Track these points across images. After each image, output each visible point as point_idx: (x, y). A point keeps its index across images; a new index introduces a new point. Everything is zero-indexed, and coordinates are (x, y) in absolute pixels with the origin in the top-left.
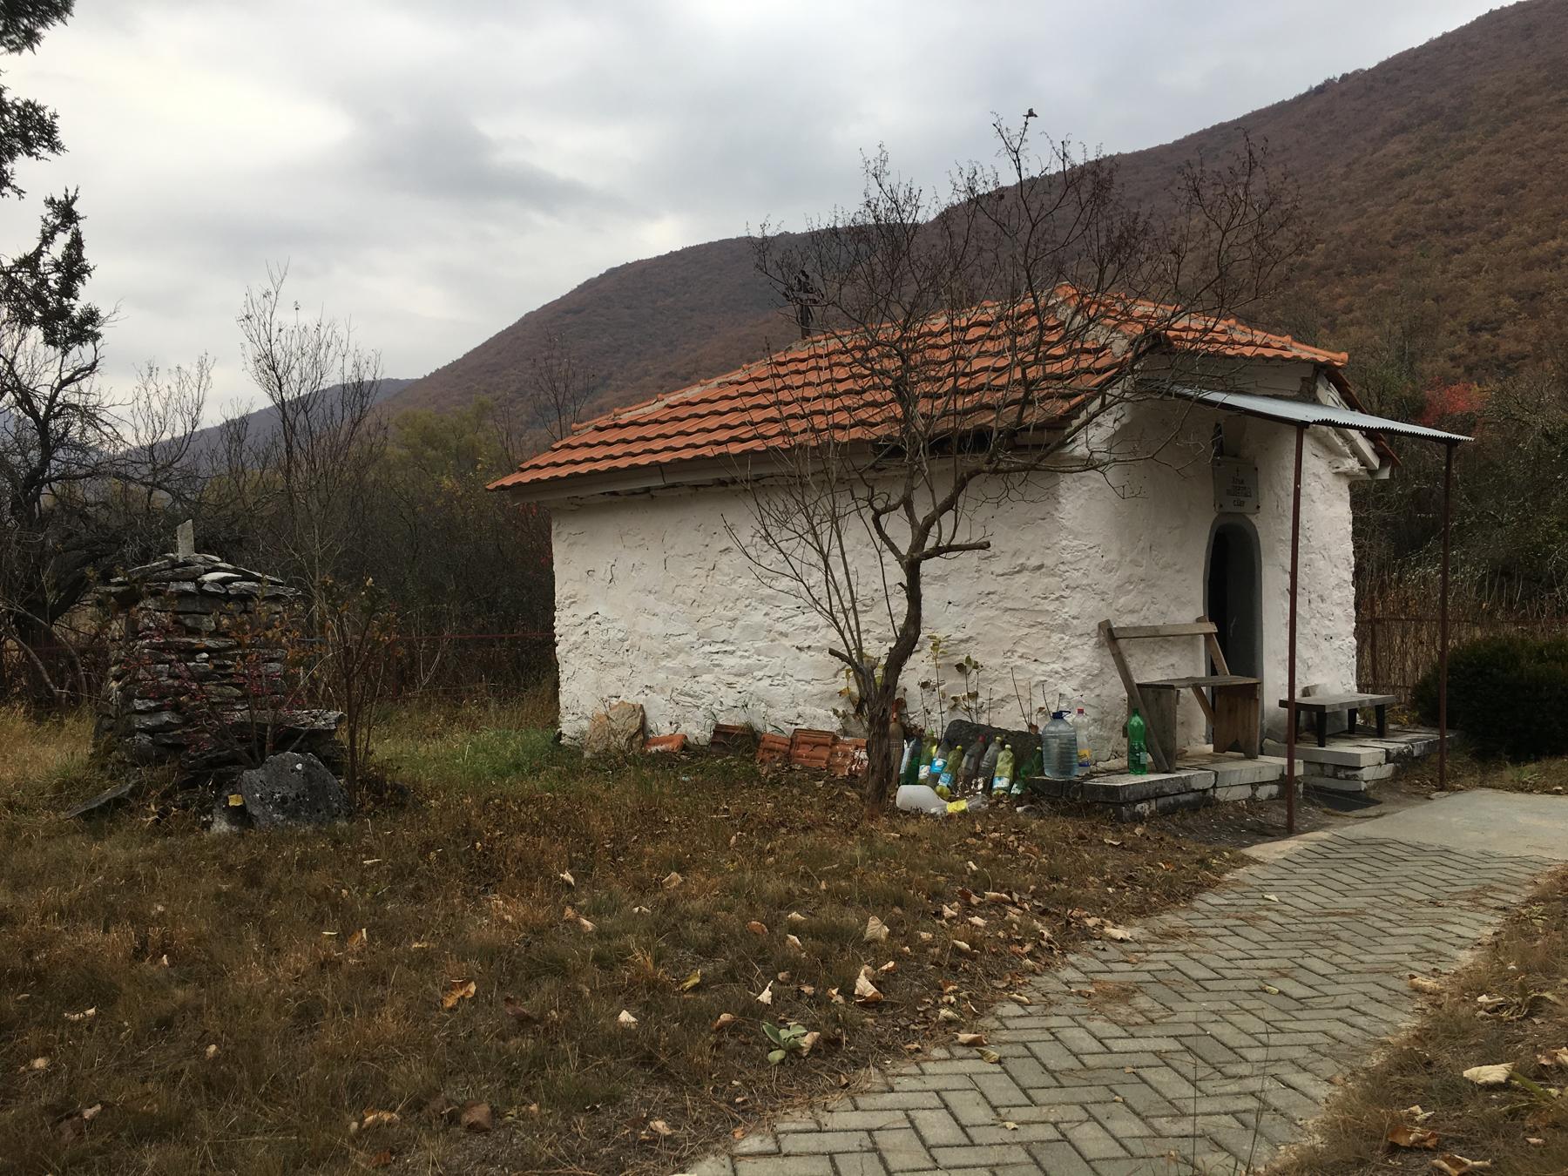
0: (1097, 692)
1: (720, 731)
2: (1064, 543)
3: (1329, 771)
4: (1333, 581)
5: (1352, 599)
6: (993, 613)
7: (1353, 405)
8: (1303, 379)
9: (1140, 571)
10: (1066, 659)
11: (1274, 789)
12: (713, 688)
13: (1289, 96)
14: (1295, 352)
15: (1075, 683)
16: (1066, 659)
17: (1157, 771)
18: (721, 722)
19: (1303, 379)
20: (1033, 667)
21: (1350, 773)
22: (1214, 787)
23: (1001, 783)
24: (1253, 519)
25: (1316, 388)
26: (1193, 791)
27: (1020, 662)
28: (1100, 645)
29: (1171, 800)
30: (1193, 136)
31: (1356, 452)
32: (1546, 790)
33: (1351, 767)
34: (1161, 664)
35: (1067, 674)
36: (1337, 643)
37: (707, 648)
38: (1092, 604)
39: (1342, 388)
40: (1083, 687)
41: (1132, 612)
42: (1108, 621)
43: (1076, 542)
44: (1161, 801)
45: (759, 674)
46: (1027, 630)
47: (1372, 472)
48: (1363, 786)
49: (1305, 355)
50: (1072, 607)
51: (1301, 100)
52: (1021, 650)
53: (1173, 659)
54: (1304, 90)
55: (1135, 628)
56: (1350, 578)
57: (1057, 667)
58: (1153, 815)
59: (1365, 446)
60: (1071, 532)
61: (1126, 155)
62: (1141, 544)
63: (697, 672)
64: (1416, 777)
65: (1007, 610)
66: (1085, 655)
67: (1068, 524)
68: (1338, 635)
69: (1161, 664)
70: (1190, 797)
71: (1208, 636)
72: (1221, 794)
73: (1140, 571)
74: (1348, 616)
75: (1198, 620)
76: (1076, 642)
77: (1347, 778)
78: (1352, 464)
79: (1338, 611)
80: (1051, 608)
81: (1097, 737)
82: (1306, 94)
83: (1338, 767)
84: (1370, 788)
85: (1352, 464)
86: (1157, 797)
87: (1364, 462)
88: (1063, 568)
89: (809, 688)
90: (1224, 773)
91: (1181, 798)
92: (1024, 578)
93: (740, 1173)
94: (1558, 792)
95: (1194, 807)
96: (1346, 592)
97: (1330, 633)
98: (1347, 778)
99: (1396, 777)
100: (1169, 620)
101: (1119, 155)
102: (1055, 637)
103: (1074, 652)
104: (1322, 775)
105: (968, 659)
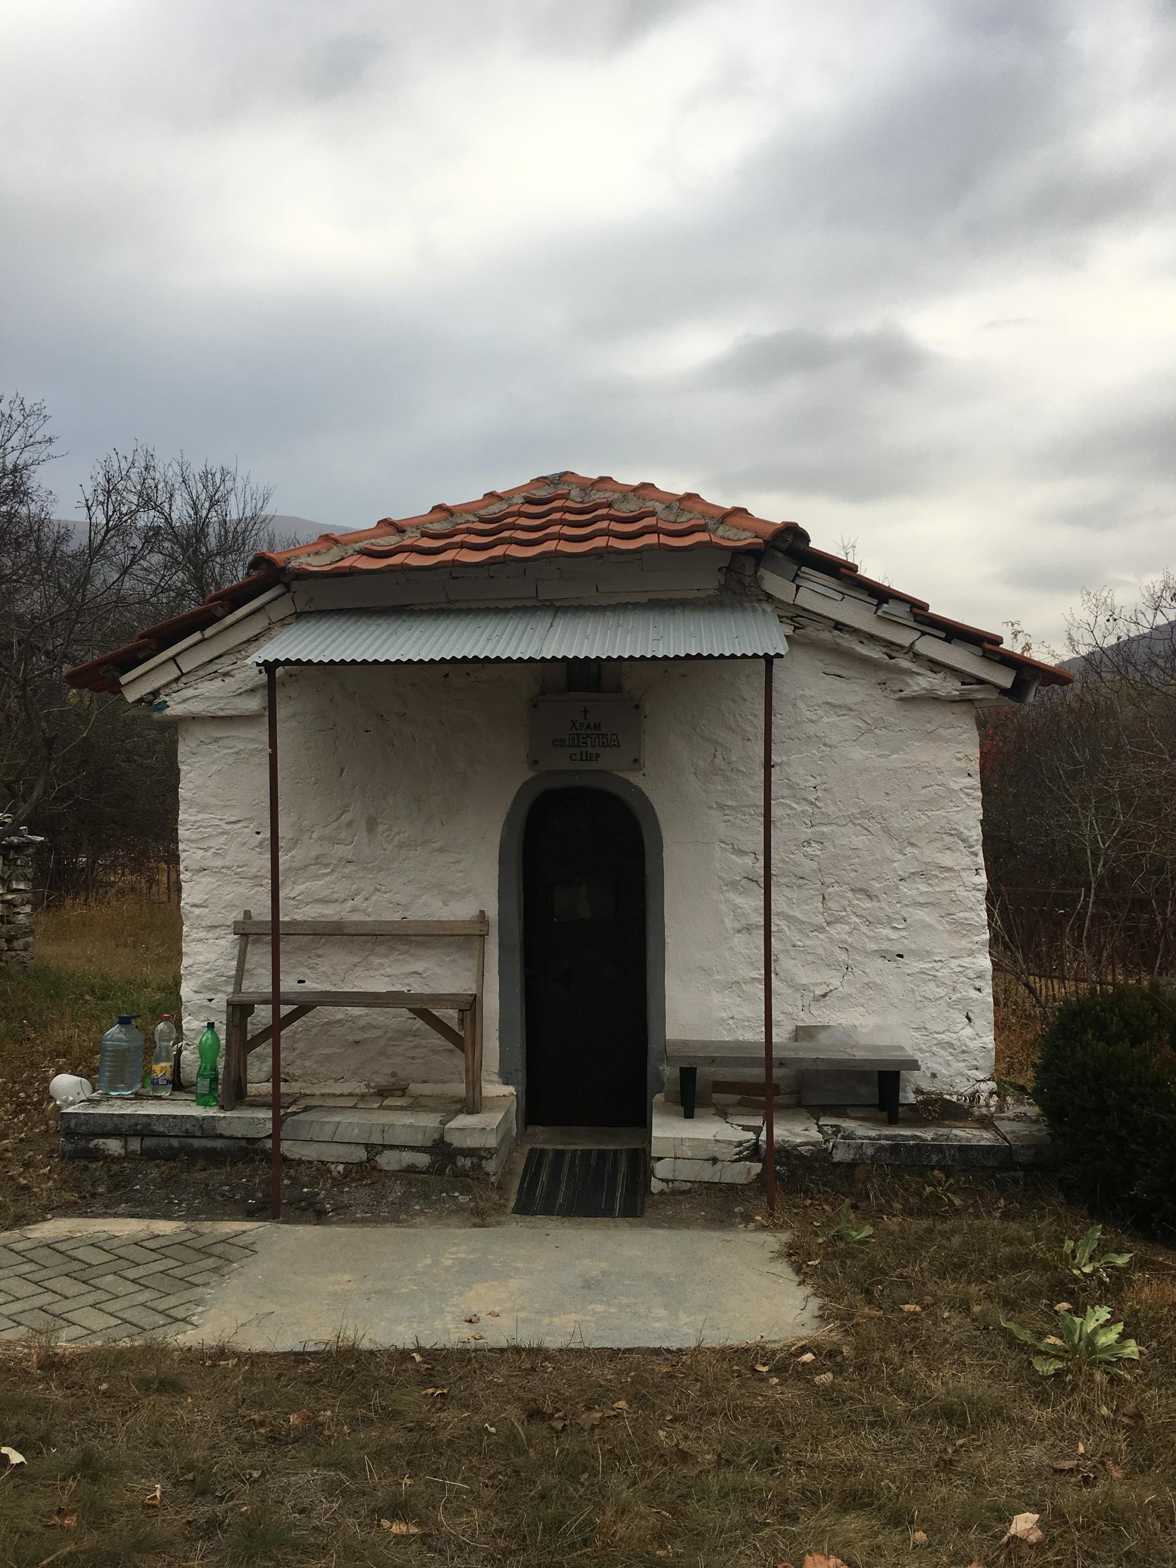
24: (635, 779)
25: (757, 581)
26: (221, 1136)
29: (175, 1143)
43: (200, 816)
44: (150, 1142)
53: (419, 966)
58: (129, 1156)
62: (346, 818)
69: (389, 971)
70: (218, 1144)
76: (202, 934)
91: (196, 1143)
95: (214, 1158)
97: (897, 948)
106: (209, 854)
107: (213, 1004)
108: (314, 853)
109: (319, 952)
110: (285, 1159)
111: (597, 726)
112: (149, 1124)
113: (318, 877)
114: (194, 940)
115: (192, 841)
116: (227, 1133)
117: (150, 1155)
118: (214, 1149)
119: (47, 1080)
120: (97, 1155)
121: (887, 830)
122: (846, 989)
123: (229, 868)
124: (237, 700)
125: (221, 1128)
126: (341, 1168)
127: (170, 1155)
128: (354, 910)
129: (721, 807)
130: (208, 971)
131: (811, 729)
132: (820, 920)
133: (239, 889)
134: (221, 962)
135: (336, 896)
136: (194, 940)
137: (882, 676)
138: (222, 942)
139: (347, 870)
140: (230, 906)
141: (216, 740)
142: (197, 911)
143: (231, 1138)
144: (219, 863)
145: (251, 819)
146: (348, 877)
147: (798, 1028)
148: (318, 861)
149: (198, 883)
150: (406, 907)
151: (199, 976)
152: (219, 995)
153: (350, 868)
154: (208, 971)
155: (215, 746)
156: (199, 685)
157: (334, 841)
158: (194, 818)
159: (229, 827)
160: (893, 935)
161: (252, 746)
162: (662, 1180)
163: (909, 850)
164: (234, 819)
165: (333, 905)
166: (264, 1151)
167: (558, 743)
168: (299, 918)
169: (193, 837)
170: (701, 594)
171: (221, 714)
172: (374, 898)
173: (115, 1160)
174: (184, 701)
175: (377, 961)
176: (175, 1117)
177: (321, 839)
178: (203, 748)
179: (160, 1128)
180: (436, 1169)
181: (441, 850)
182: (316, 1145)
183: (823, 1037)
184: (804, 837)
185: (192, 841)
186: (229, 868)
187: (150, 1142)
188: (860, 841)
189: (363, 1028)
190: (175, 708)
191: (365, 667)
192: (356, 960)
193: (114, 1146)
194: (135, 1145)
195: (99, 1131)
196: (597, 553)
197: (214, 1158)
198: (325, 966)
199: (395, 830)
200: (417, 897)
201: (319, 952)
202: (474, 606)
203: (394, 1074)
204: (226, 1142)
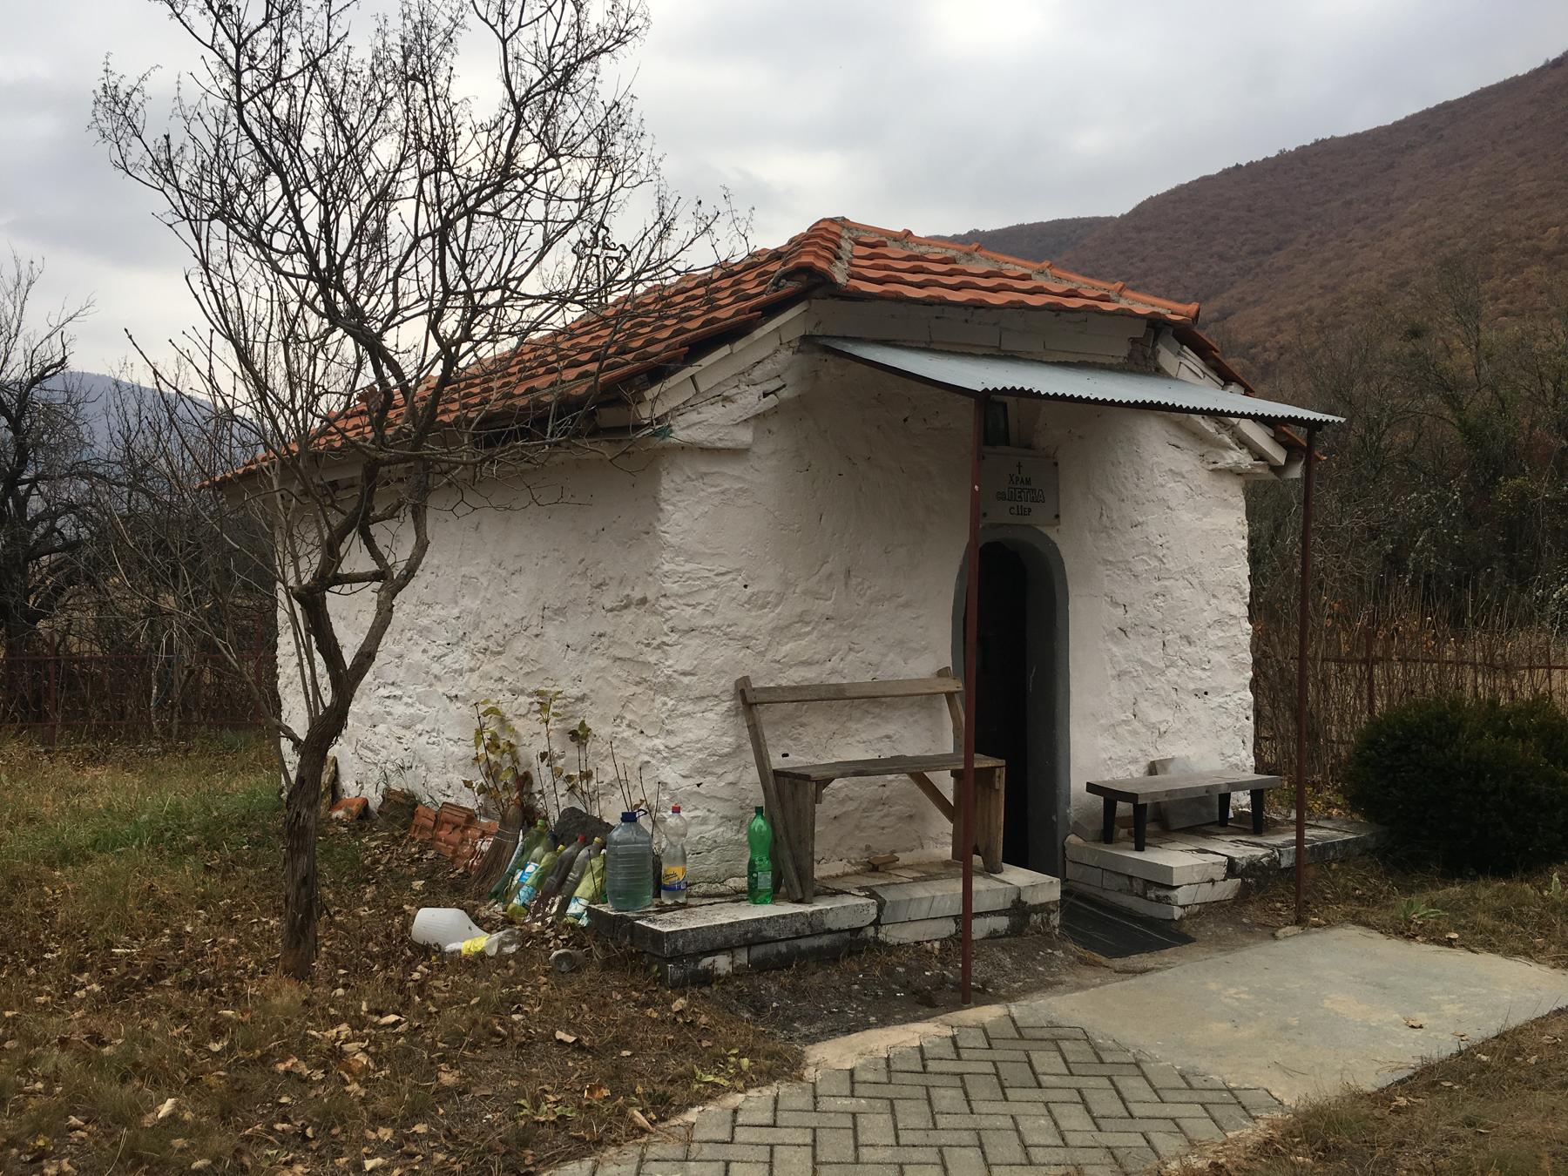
0: (730, 778)
1: (388, 795)
2: (666, 567)
3: (1137, 887)
4: (1209, 616)
5: (1246, 640)
6: (602, 662)
7: (1227, 378)
8: (1134, 341)
9: (825, 607)
10: (669, 732)
11: (1002, 923)
12: (386, 743)
13: (1522, 70)
14: (1123, 304)
15: (683, 767)
16: (669, 732)
17: (776, 896)
18: (394, 786)
19: (1134, 341)
20: (638, 741)
21: (1162, 893)
22: (876, 923)
23: (574, 908)
24: (1051, 533)
25: (1155, 354)
26: (830, 931)
27: (628, 733)
28: (733, 713)
29: (783, 947)
30: (1414, 116)
31: (1243, 442)
32: (1437, 938)
33: (1160, 884)
34: (864, 736)
35: (674, 754)
36: (1215, 700)
37: (383, 692)
38: (722, 655)
39: (1203, 351)
40: (702, 770)
41: (807, 663)
42: (746, 679)
43: (688, 567)
44: (758, 951)
45: (419, 727)
46: (634, 689)
47: (1276, 469)
48: (1177, 913)
49: (1140, 309)
50: (679, 658)
51: (1536, 74)
52: (629, 716)
53: (890, 729)
54: (1539, 64)
55: (794, 688)
56: (1244, 611)
57: (658, 743)
58: (738, 973)
59: (1259, 436)
60: (678, 551)
61: (1340, 139)
62: (827, 568)
63: (375, 720)
64: (1275, 898)
65: (617, 659)
66: (709, 727)
67: (675, 540)
68: (1220, 690)
69: (864, 736)
70: (825, 941)
71: (950, 696)
72: (893, 934)
73: (825, 607)
74: (1240, 663)
75: (942, 673)
76: (689, 708)
77: (1158, 899)
78: (1237, 457)
79: (1218, 657)
80: (652, 660)
81: (730, 842)
82: (1543, 68)
83: (1149, 884)
84: (1190, 916)
85: (1237, 457)
86: (749, 945)
87: (1259, 455)
88: (664, 603)
89: (455, 749)
90: (896, 904)
91: (804, 944)
92: (628, 616)
93: (951, 1171)
94: (1450, 943)
95: (827, 957)
96: (1235, 631)
97: (1205, 688)
98: (1158, 899)
99: (1242, 897)
100: (884, 674)
101: (1333, 138)
102: (660, 699)
103: (686, 723)
104: (1130, 892)
105: (583, 724)
106: (697, 612)
107: (701, 790)
108: (799, 610)
109: (803, 720)
110: (884, 944)
111: (1028, 481)
112: (760, 930)
113: (800, 636)
114: (682, 715)
115: (680, 596)
116: (834, 927)
117: (761, 967)
118: (820, 947)
119: (409, 919)
120: (707, 978)
121: (1201, 584)
122: (1178, 725)
123: (718, 628)
124: (735, 430)
125: (831, 923)
126: (937, 945)
127: (783, 962)
128: (833, 672)
129: (1106, 562)
130: (699, 750)
131: (1161, 493)
132: (1161, 665)
133: (729, 652)
134: (713, 739)
135: (816, 657)
136: (682, 715)
137: (1204, 449)
138: (710, 715)
139: (826, 628)
140: (720, 672)
141: (703, 476)
142: (686, 680)
143: (840, 931)
144: (708, 622)
145: (739, 570)
146: (827, 636)
147: (1153, 763)
148: (802, 619)
149: (685, 646)
150: (877, 666)
151: (690, 757)
152: (709, 778)
153: (831, 625)
154: (699, 750)
155: (699, 484)
156: (703, 409)
157: (817, 596)
158: (682, 569)
159: (718, 579)
160: (1204, 675)
161: (738, 486)
162: (1183, 907)
163: (1213, 601)
164: (723, 570)
165: (814, 668)
166: (866, 941)
167: (1001, 496)
168: (784, 683)
169: (682, 591)
170: (1114, 361)
171: (719, 445)
172: (849, 658)
173: (727, 979)
174: (688, 427)
175: (854, 726)
176: (784, 917)
177: (805, 593)
178: (689, 485)
179: (770, 932)
180: (1015, 931)
181: (906, 605)
182: (912, 925)
183: (1171, 767)
184: (1155, 590)
185: (680, 596)
186: (718, 628)
187: (758, 951)
188: (1187, 594)
189: (842, 802)
190: (680, 435)
191: (1079, 405)
192: (834, 727)
193: (722, 963)
194: (743, 958)
195: (708, 947)
196: (1012, 305)
197: (827, 957)
198: (808, 736)
199: (867, 583)
200: (885, 655)
201: (803, 720)
202: (952, 349)
203: (868, 848)
204: (834, 937)
